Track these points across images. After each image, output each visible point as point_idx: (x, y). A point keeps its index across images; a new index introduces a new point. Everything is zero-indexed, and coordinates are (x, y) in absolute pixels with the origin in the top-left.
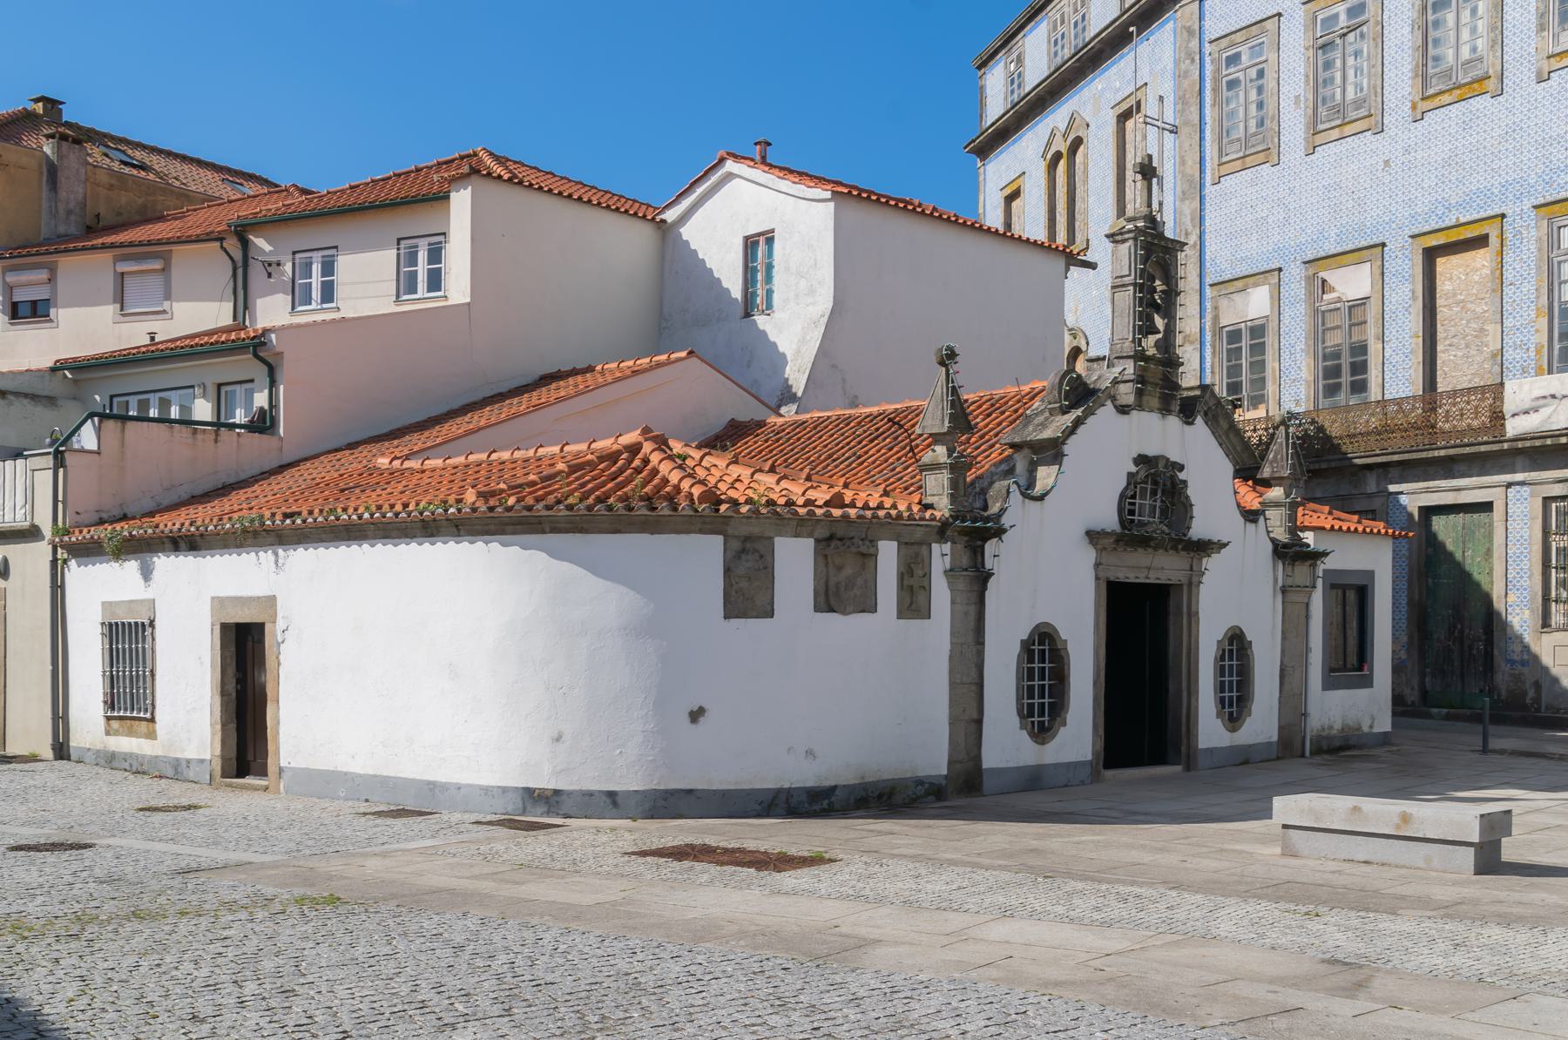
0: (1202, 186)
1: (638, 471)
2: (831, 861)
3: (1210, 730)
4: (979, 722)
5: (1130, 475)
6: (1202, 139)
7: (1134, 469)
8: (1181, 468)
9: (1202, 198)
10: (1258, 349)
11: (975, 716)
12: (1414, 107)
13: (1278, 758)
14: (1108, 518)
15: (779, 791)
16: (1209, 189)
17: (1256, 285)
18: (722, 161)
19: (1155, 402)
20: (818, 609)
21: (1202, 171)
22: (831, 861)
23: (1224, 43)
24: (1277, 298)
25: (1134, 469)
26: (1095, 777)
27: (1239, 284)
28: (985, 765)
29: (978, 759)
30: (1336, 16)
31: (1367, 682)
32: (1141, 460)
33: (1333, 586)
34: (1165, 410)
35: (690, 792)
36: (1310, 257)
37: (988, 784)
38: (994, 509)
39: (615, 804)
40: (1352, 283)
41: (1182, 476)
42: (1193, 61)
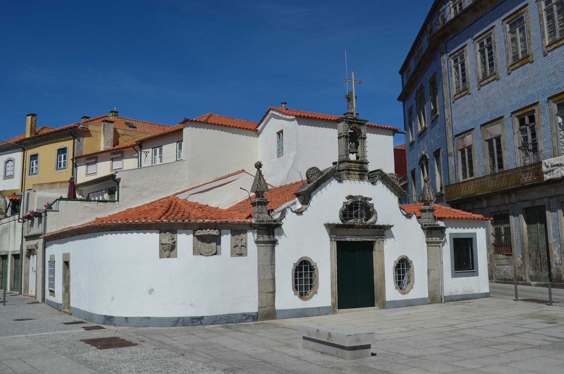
1: (178, 212)
2: (82, 341)
3: (391, 292)
7: (346, 201)
8: (371, 199)
11: (271, 290)
12: (508, 69)
13: (429, 303)
14: (336, 220)
15: (179, 318)
18: (268, 112)
19: (345, 176)
22: (82, 341)
25: (346, 201)
26: (334, 312)
28: (277, 309)
29: (274, 305)
31: (476, 274)
32: (350, 197)
34: (361, 178)
35: (149, 318)
36: (482, 123)
37: (278, 315)
38: (276, 216)
39: (127, 322)
40: (496, 130)
41: (370, 202)
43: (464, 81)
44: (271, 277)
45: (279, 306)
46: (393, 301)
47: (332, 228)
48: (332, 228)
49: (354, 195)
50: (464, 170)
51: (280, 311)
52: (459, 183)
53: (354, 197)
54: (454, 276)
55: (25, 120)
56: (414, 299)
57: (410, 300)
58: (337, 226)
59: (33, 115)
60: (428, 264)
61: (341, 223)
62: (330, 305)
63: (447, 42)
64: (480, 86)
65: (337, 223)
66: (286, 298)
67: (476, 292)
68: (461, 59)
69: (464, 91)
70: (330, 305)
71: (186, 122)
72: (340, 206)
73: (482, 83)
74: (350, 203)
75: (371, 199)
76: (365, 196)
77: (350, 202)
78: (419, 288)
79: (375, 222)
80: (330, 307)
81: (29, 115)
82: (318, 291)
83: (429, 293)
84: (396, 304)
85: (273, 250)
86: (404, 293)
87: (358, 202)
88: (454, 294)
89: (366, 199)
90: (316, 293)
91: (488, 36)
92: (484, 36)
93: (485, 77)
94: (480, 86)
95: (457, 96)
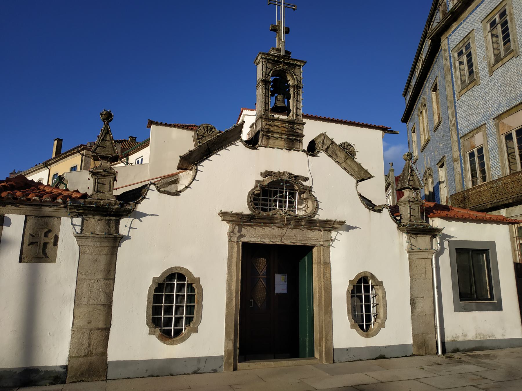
0: (455, 102)
3: (344, 334)
4: (106, 329)
5: (257, 182)
6: (453, 85)
7: (261, 179)
8: (306, 179)
9: (455, 107)
10: (481, 158)
11: (101, 325)
16: (457, 102)
17: (477, 133)
20: (456, 311)
21: (454, 97)
23: (456, 49)
24: (485, 136)
25: (261, 179)
27: (471, 134)
28: (110, 358)
29: (104, 354)
30: (495, 19)
33: (457, 250)
42: (447, 59)
43: (471, 72)
44: (103, 299)
45: (114, 354)
46: (347, 350)
47: (236, 220)
48: (236, 220)
49: (275, 170)
50: (474, 176)
51: (119, 364)
52: (468, 190)
53: (275, 173)
54: (457, 309)
55: (53, 144)
56: (386, 347)
57: (379, 347)
58: (241, 216)
59: (60, 140)
60: (412, 288)
61: (248, 211)
62: (223, 354)
63: (450, 36)
64: (491, 72)
65: (238, 211)
66: (132, 340)
67: (499, 337)
68: (466, 50)
69: (471, 78)
70: (223, 354)
71: (151, 123)
72: (249, 186)
73: (494, 68)
74: (266, 183)
75: (306, 179)
76: (296, 174)
77: (267, 181)
78: (396, 329)
79: (315, 214)
80: (222, 357)
81: (55, 140)
82: (200, 328)
83: (414, 336)
84: (354, 357)
85: (113, 254)
86: (368, 336)
87: (282, 181)
88: (461, 339)
89: (296, 177)
90: (196, 331)
91: (502, 11)
92: (495, 12)
93: (498, 59)
94: (491, 72)
95: (463, 92)
